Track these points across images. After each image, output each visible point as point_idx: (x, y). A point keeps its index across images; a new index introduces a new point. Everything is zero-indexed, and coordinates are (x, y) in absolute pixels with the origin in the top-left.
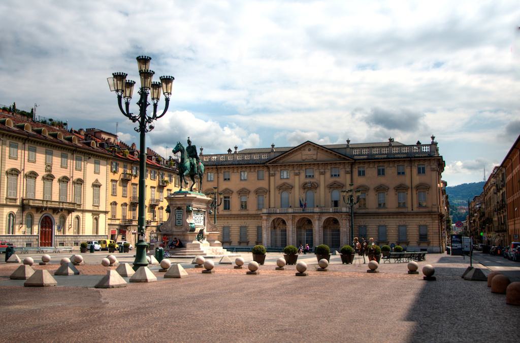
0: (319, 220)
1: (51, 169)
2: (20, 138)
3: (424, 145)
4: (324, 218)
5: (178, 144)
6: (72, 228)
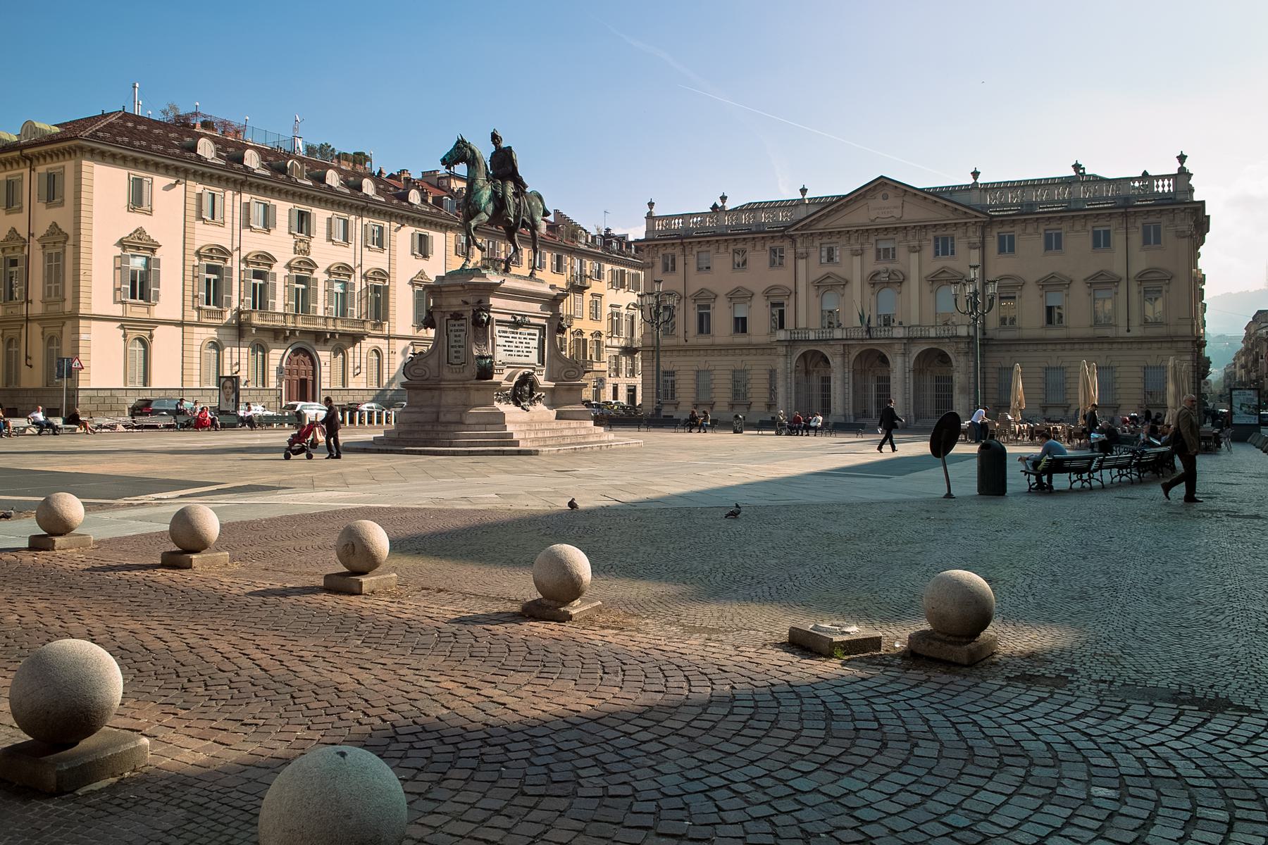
0: (904, 354)
1: (309, 246)
2: (227, 180)
3: (1158, 178)
4: (916, 350)
5: (458, 142)
6: (363, 375)
